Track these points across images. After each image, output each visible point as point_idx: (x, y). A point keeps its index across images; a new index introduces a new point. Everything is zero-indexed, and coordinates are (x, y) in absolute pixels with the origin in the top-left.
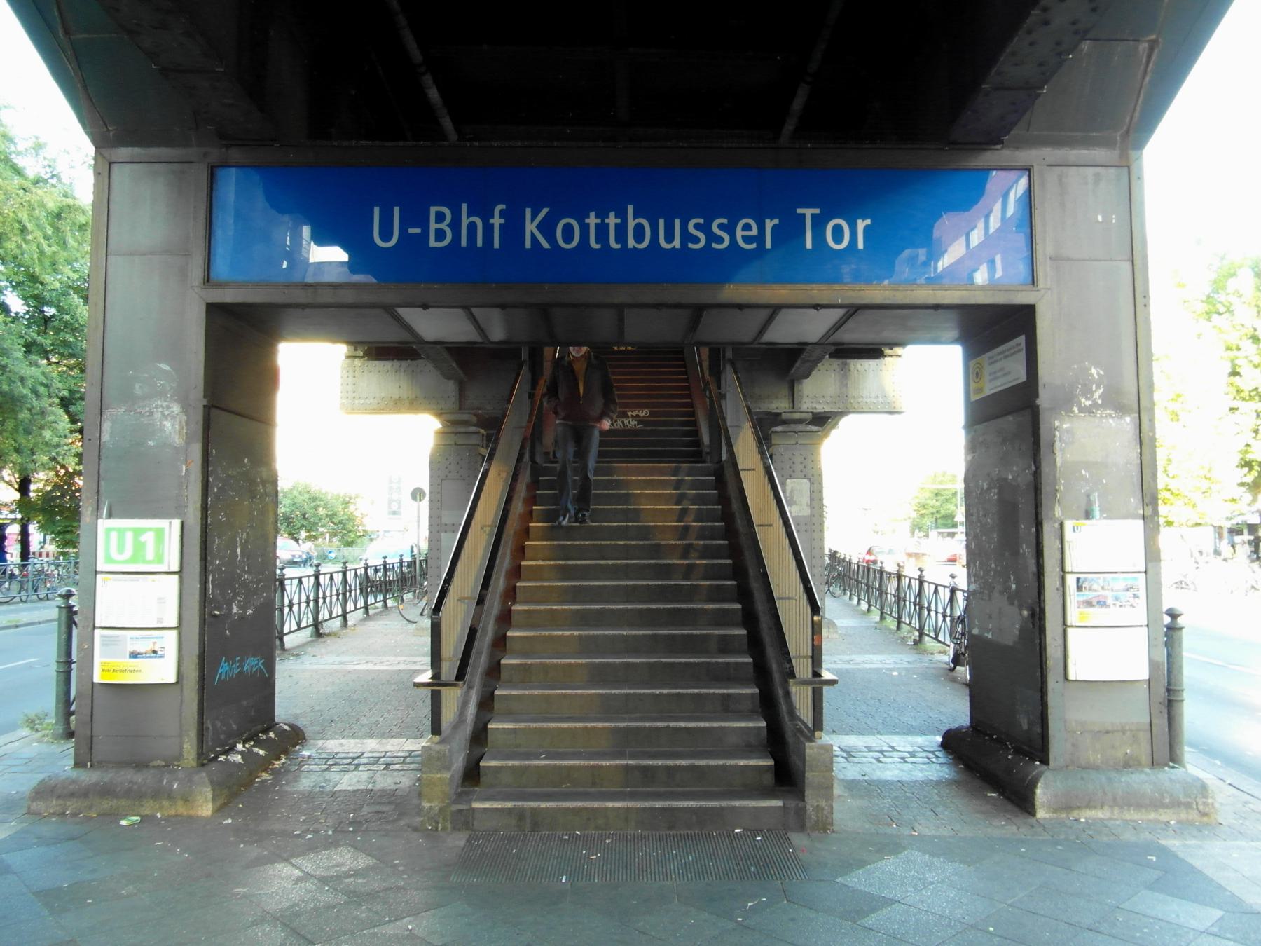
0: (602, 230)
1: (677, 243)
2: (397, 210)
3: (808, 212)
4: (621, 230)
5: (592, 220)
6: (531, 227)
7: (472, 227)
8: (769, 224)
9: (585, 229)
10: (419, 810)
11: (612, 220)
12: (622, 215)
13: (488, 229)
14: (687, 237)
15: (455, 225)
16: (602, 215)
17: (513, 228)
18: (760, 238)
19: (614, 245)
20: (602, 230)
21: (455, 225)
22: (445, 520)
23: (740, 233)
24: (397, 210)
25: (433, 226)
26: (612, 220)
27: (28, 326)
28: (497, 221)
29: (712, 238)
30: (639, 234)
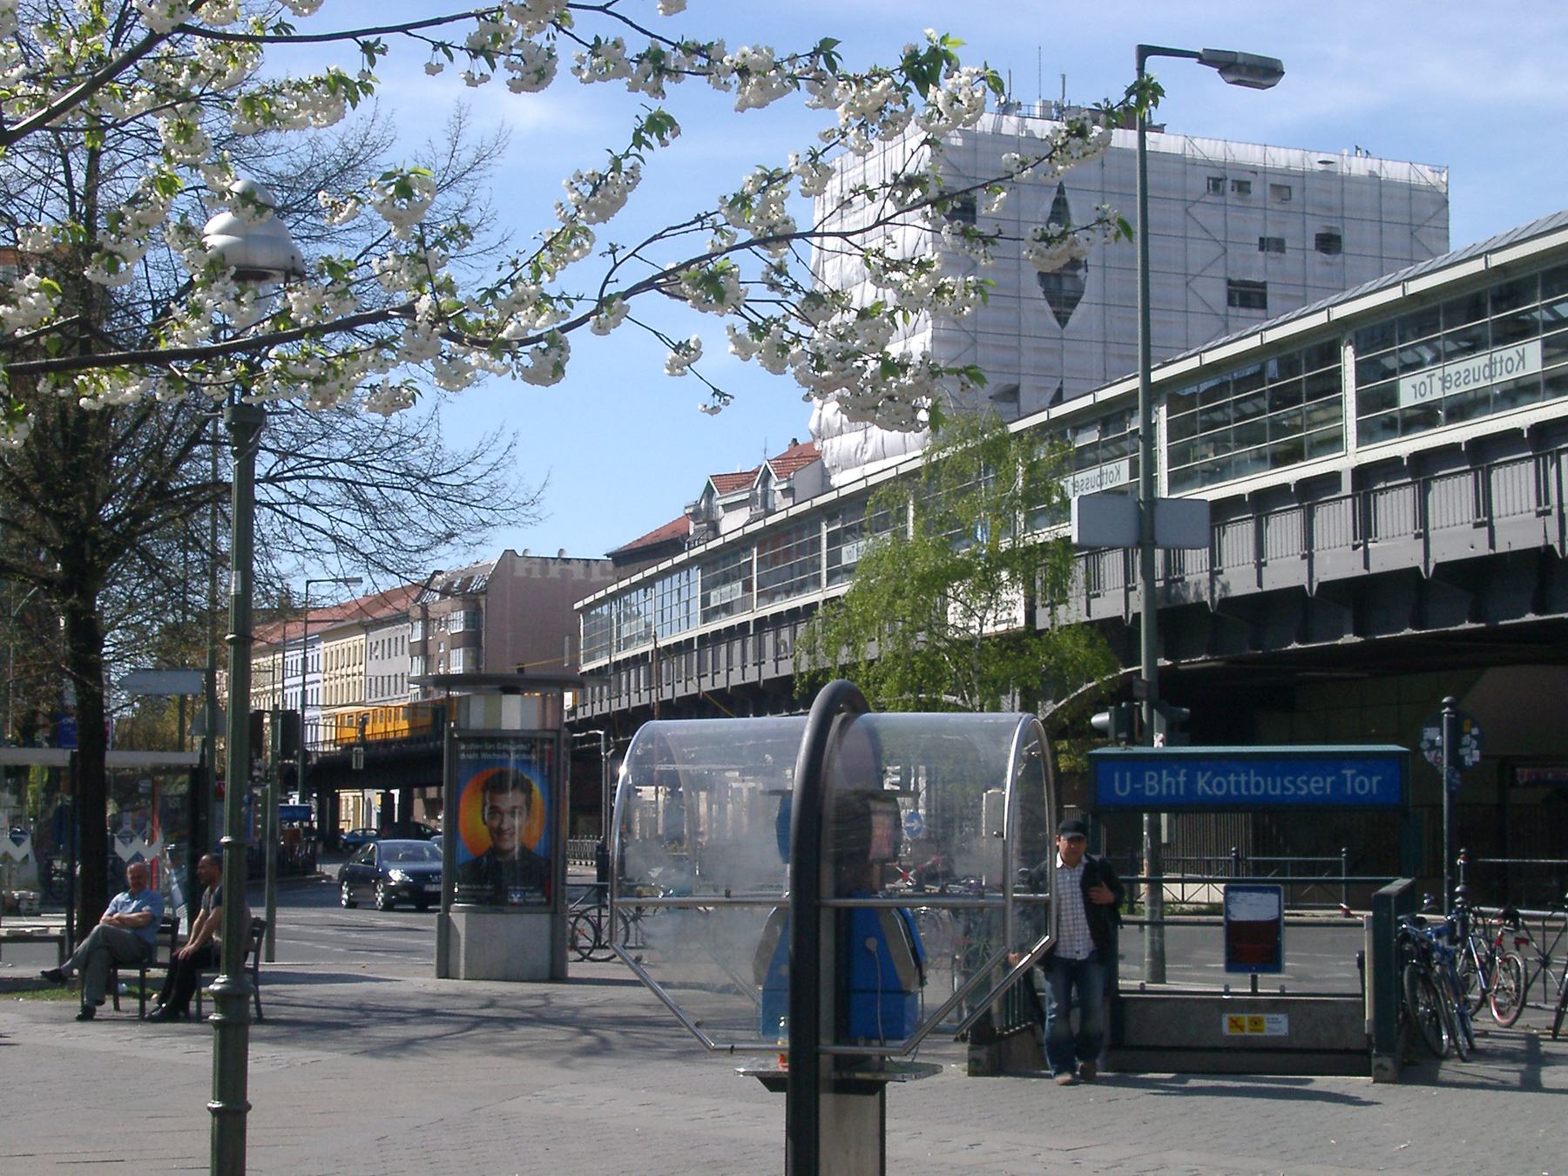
0: (1238, 784)
1: (1278, 792)
2: (1128, 774)
3: (1349, 773)
4: (1248, 783)
5: (1232, 778)
6: (1201, 783)
7: (1169, 785)
8: (1329, 780)
9: (1228, 783)
10: (93, 554)
11: (1243, 778)
12: (1248, 775)
13: (1177, 784)
14: (1284, 788)
15: (1160, 782)
16: (1237, 775)
17: (1191, 782)
18: (1323, 788)
19: (1243, 791)
20: (1238, 784)
21: (1160, 782)
22: (994, 204)
23: (1313, 785)
24: (1128, 774)
25: (1147, 783)
26: (1243, 778)
27: (648, 626)
28: (1182, 779)
29: (1293, 783)
30: (1257, 786)
